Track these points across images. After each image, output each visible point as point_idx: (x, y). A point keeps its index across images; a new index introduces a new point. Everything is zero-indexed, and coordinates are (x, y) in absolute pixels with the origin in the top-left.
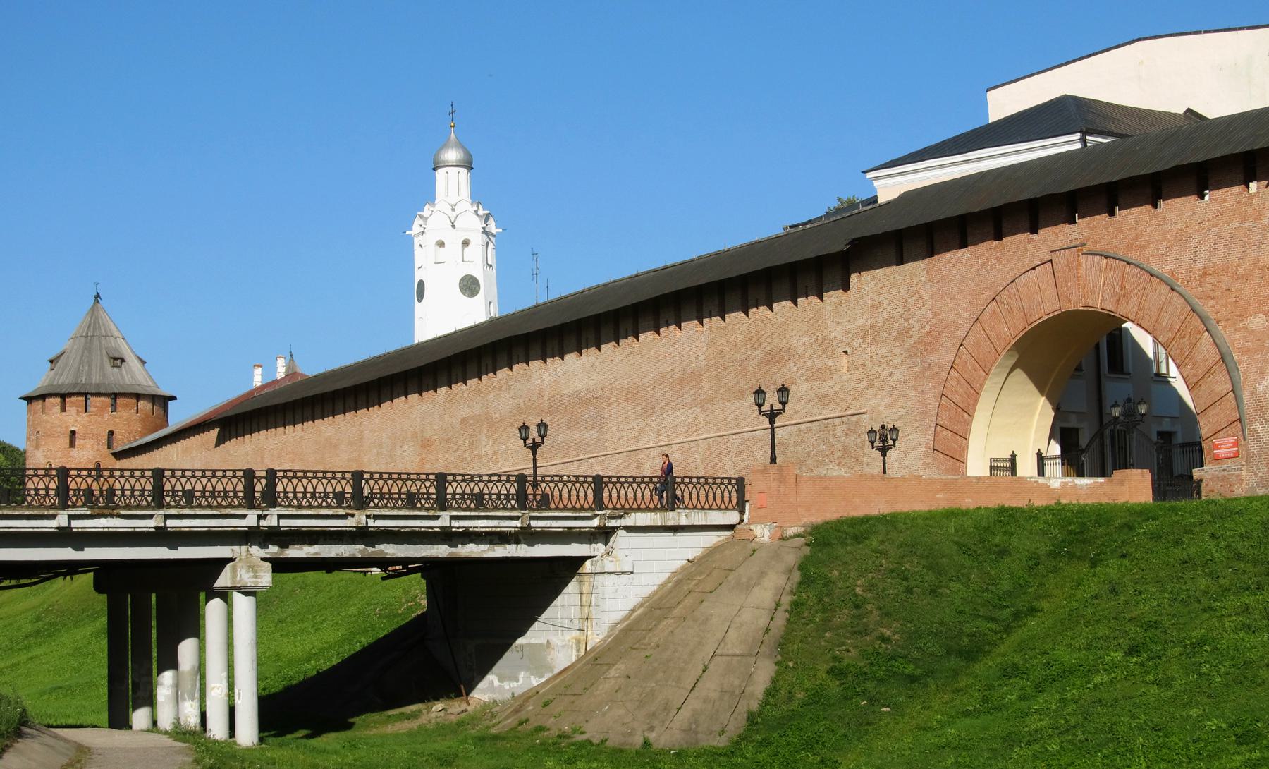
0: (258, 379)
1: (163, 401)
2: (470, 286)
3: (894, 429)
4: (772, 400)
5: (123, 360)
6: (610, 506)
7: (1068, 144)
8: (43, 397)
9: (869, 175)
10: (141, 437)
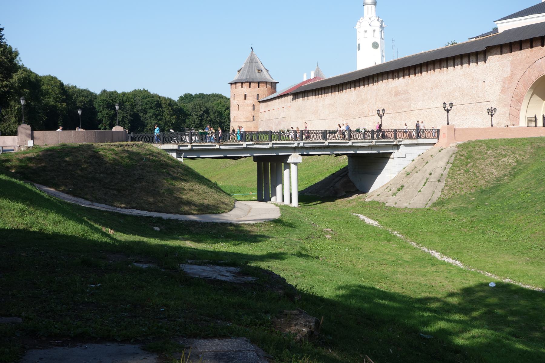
1: (274, 85)
2: (375, 45)
3: (495, 109)
4: (448, 107)
5: (261, 71)
8: (236, 83)
9: (496, 23)
10: (268, 95)
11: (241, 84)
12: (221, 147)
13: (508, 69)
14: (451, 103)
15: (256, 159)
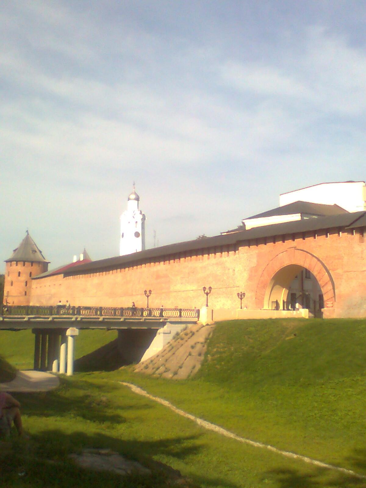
0: (75, 260)
3: (244, 293)
6: (125, 315)
7: (296, 217)
11: (15, 262)
12: (5, 320)
13: (255, 260)
14: (210, 288)
15: (35, 331)
